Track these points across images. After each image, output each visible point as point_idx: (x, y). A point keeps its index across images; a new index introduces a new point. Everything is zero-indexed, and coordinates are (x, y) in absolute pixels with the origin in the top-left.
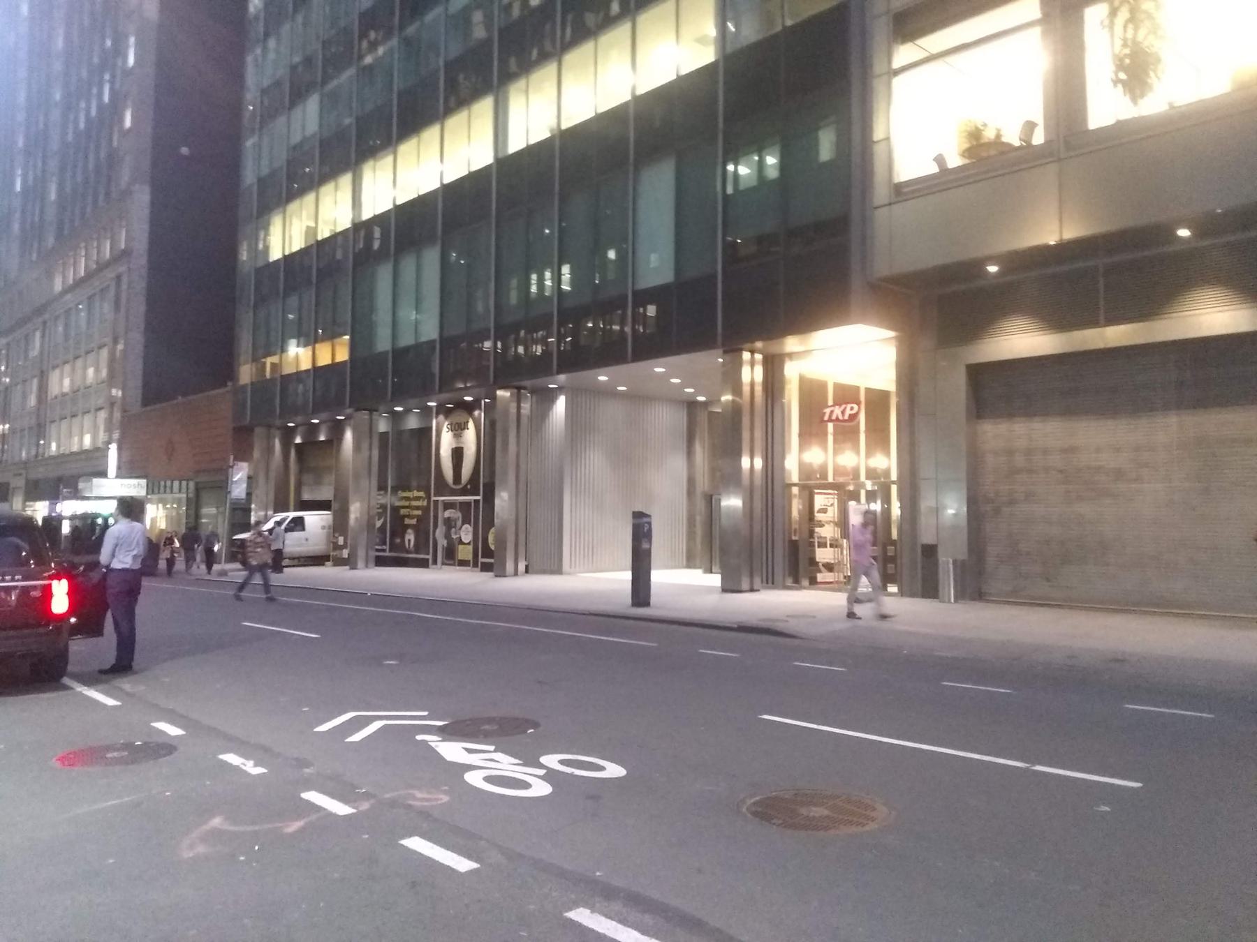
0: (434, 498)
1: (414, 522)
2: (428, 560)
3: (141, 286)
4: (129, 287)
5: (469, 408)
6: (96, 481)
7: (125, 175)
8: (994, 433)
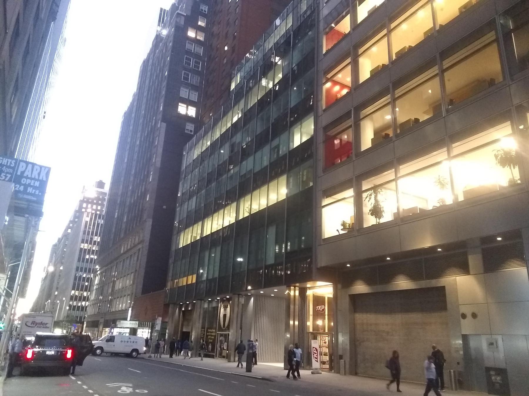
0: (217, 332)
1: (211, 341)
2: (214, 355)
3: (146, 252)
4: (142, 253)
5: (228, 300)
6: (122, 321)
7: (145, 216)
8: (361, 317)
